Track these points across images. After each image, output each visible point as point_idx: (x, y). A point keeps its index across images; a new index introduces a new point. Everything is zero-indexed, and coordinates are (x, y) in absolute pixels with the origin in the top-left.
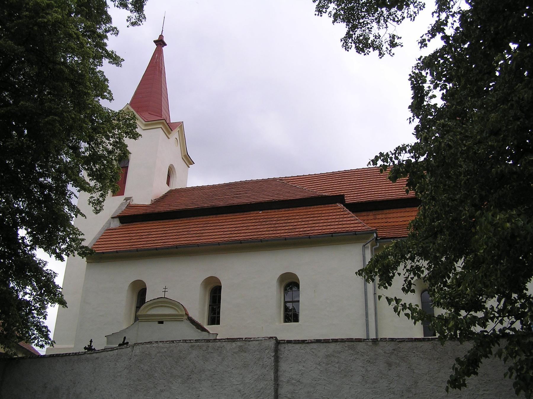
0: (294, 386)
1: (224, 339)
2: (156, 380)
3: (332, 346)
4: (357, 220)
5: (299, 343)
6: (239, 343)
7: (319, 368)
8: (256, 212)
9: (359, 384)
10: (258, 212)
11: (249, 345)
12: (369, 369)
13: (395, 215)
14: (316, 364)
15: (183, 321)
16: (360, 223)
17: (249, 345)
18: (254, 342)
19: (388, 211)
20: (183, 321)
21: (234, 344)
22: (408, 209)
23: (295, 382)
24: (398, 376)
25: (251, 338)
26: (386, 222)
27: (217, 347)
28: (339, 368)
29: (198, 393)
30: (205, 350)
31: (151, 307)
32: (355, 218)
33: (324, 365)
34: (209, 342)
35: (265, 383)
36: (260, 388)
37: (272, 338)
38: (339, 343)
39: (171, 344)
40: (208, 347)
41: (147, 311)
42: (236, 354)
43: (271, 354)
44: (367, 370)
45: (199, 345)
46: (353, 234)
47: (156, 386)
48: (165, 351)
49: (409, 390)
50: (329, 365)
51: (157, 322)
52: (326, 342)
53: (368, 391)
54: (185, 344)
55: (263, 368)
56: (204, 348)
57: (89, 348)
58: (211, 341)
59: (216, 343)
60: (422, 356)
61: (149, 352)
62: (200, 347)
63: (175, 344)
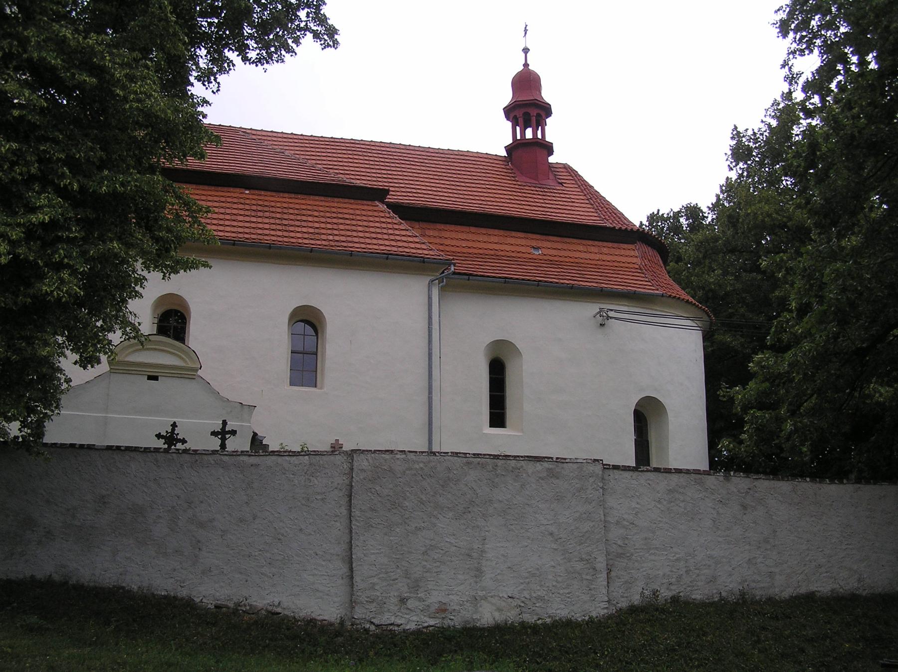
0: (627, 529)
1: (522, 457)
2: (407, 512)
3: (675, 477)
4: (417, 236)
5: (629, 470)
6: (546, 465)
7: (659, 506)
8: (238, 190)
9: (708, 531)
10: (242, 190)
11: (563, 468)
12: (721, 511)
13: (453, 235)
14: (655, 501)
15: (194, 379)
16: (424, 243)
17: (563, 468)
18: (571, 464)
19: (442, 226)
20: (194, 379)
21: (539, 466)
22: (473, 229)
23: (628, 524)
24: (755, 522)
25: (565, 459)
26: (442, 245)
27: (511, 468)
28: (685, 509)
29: (483, 534)
30: (492, 471)
31: (134, 349)
32: (413, 233)
33: (665, 503)
34: (498, 459)
35: (592, 524)
36: (585, 531)
37: (598, 460)
38: (683, 474)
39: (432, 458)
40: (497, 466)
41: (127, 355)
42: (543, 479)
43: (599, 484)
44: (718, 513)
45: (481, 463)
46: (420, 262)
47: (407, 521)
48: (421, 468)
49: (766, 541)
50: (672, 504)
51: (147, 376)
52: (666, 472)
53: (720, 539)
54: (456, 458)
55: (587, 503)
56: (490, 468)
57: (171, 438)
58: (500, 458)
59: (509, 462)
60: (781, 499)
61: (390, 467)
62: (483, 466)
63: (438, 458)
